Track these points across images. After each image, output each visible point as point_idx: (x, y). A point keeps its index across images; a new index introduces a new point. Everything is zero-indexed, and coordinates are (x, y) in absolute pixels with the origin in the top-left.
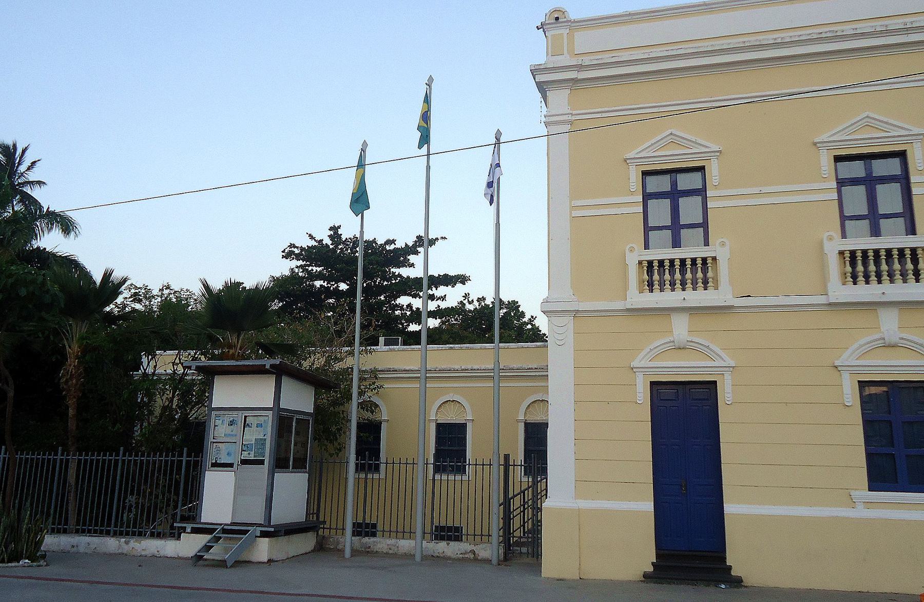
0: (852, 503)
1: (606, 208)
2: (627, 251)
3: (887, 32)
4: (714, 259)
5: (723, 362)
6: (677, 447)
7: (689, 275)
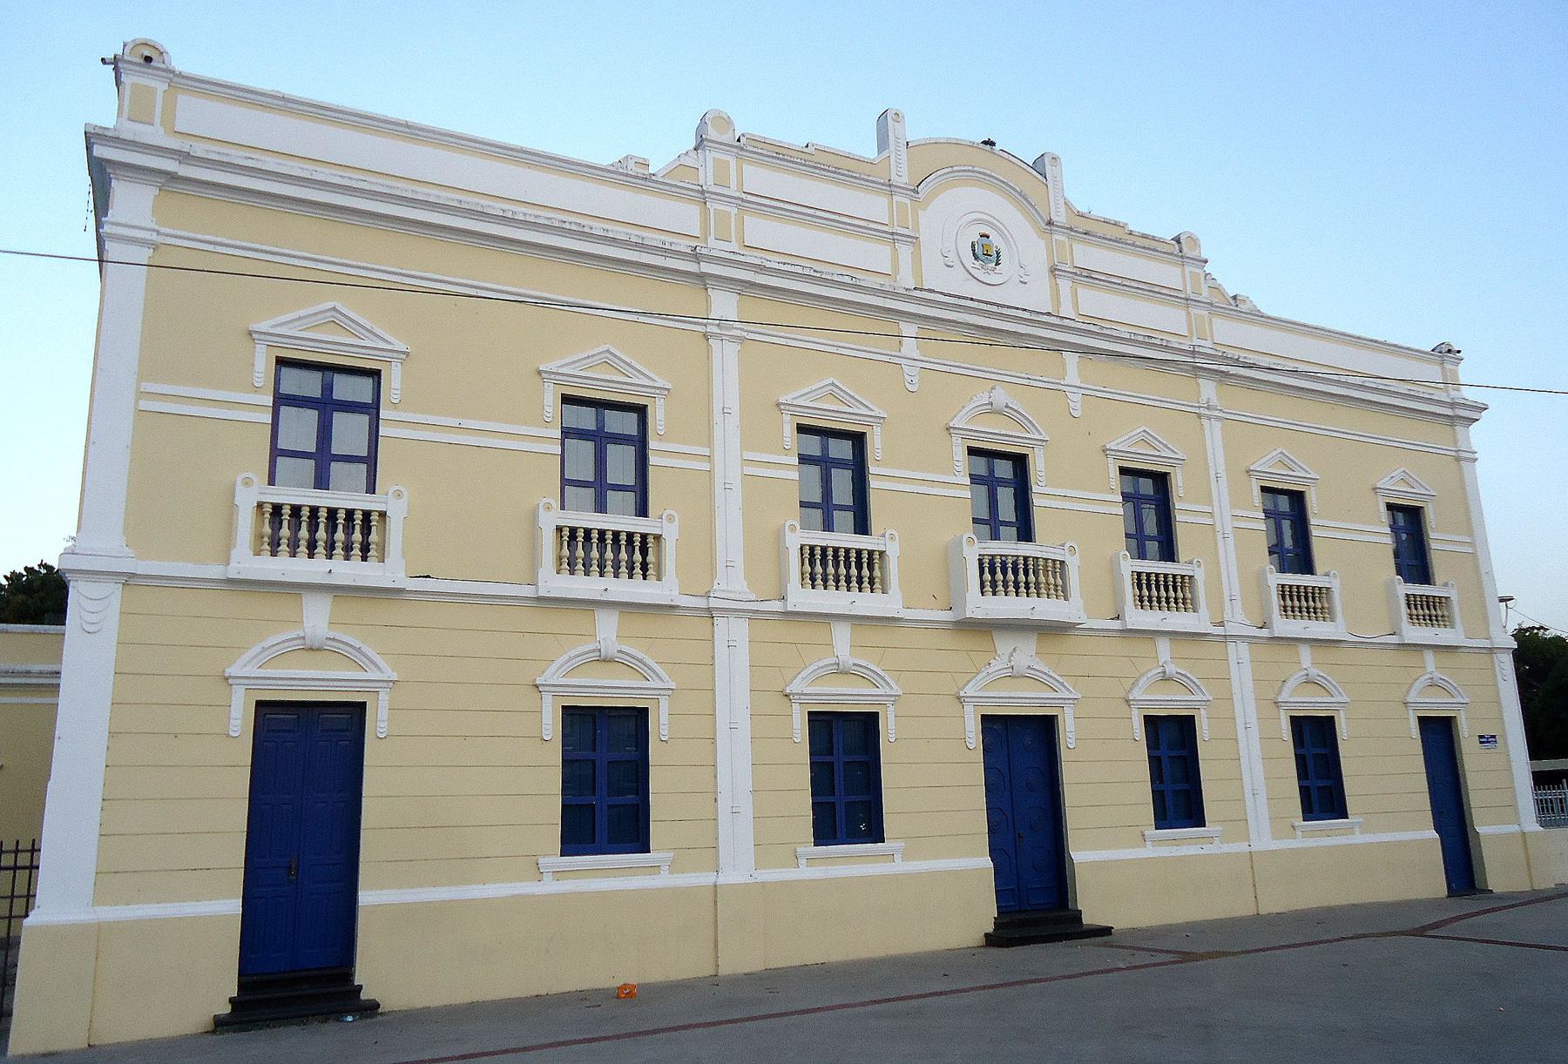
0: (539, 874)
1: (889, 481)
2: (239, 482)
3: (640, 246)
4: (383, 515)
5: (379, 674)
6: (323, 805)
7: (340, 535)
